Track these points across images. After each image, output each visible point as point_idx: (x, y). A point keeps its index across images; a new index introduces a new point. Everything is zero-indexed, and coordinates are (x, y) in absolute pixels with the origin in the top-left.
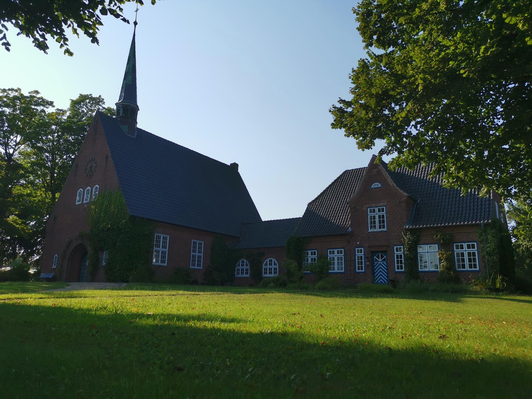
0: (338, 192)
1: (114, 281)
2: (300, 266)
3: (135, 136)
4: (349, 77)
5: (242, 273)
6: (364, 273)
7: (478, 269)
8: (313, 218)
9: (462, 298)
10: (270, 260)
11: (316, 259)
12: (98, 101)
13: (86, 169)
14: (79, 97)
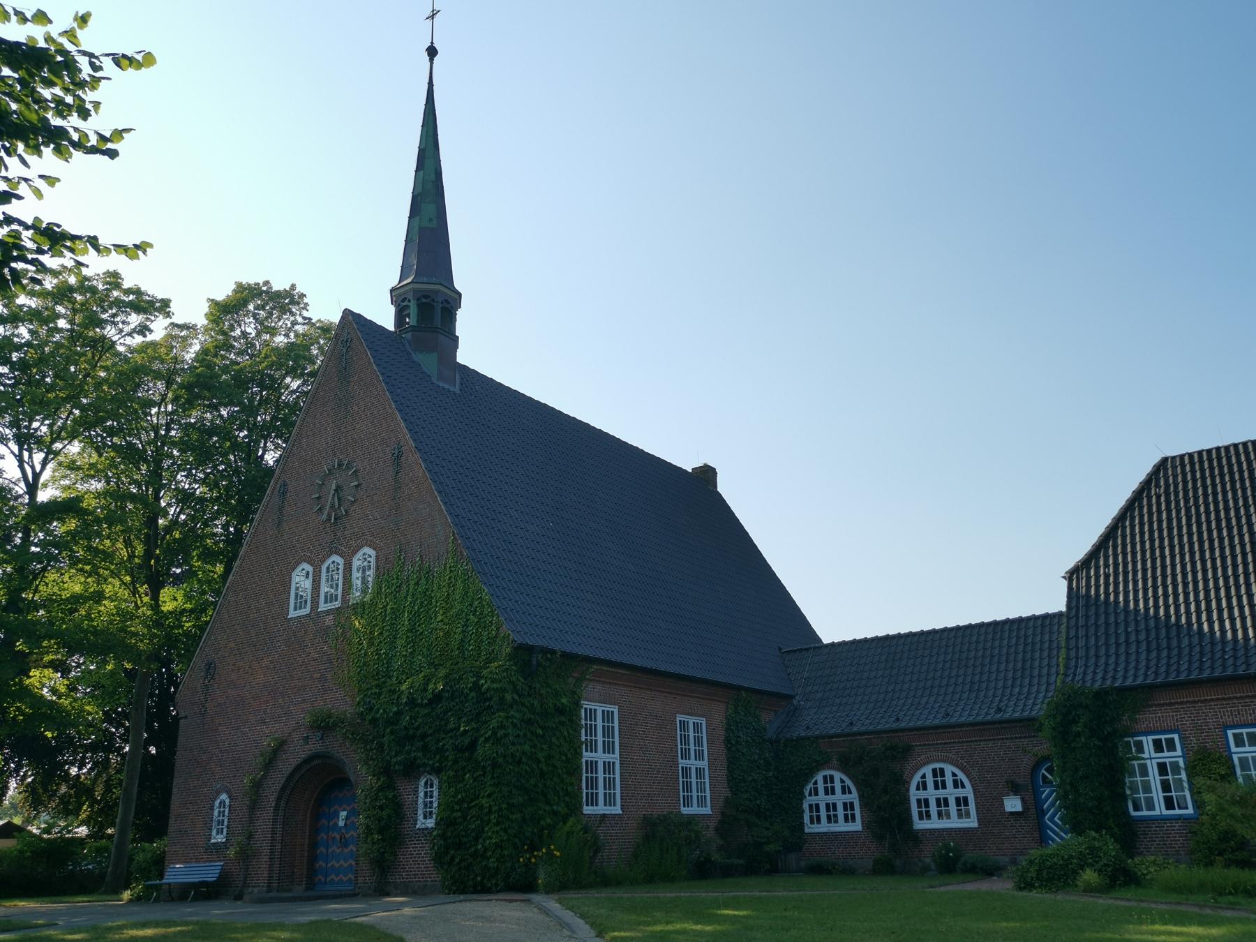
1: (463, 892)
10: (934, 771)
12: (287, 301)
13: (319, 498)
14: (234, 290)
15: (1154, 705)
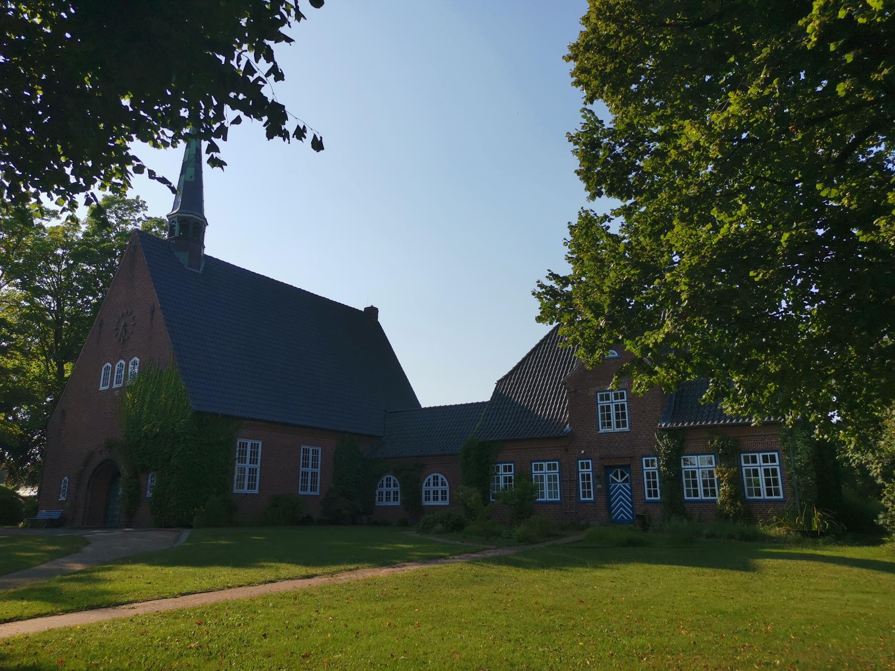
0: (547, 361)
2: (485, 494)
3: (201, 269)
4: (565, 243)
5: (388, 499)
6: (594, 503)
7: (781, 497)
8: (505, 417)
9: (757, 560)
10: (434, 477)
11: (513, 478)
13: (117, 329)
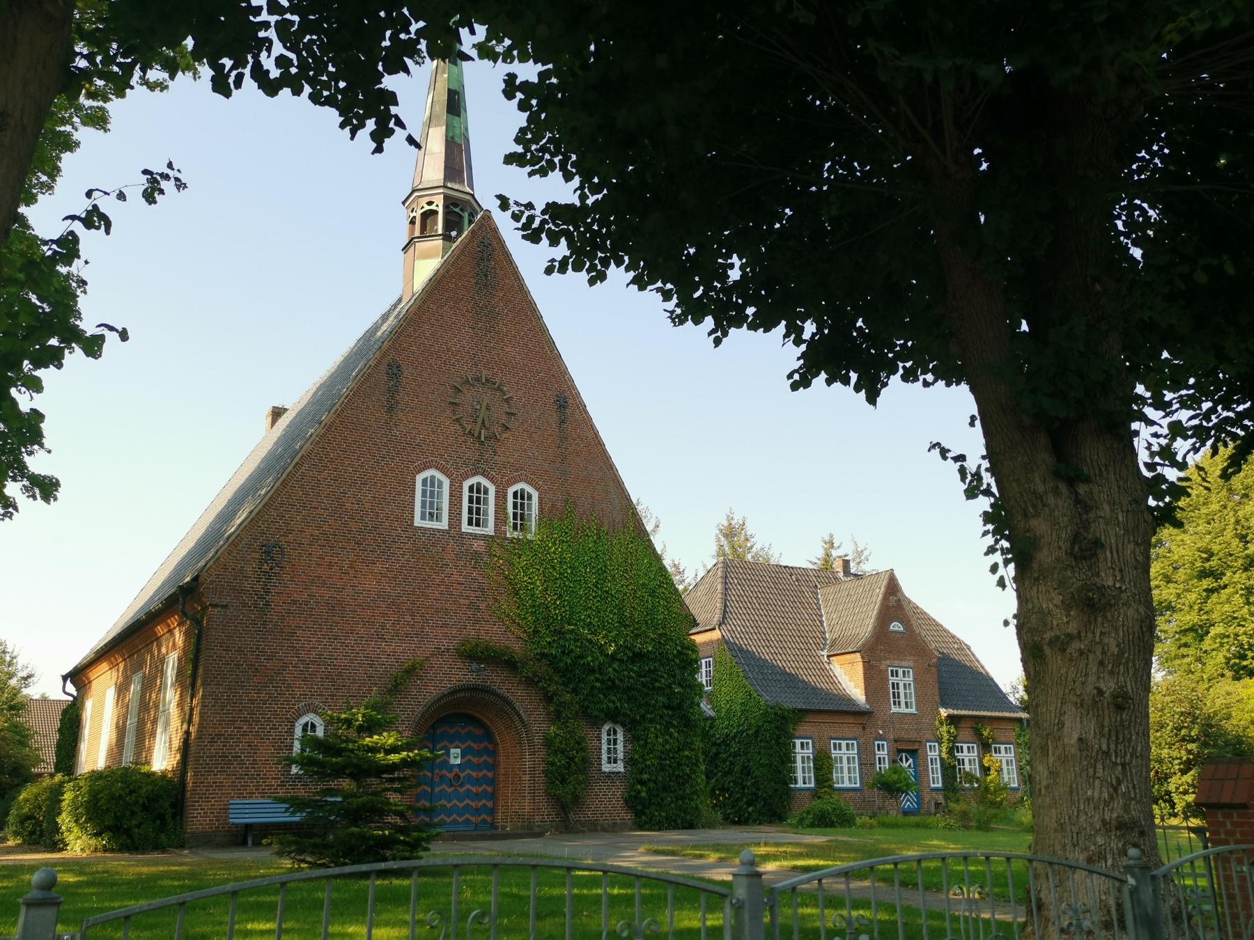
15: (940, 653)
